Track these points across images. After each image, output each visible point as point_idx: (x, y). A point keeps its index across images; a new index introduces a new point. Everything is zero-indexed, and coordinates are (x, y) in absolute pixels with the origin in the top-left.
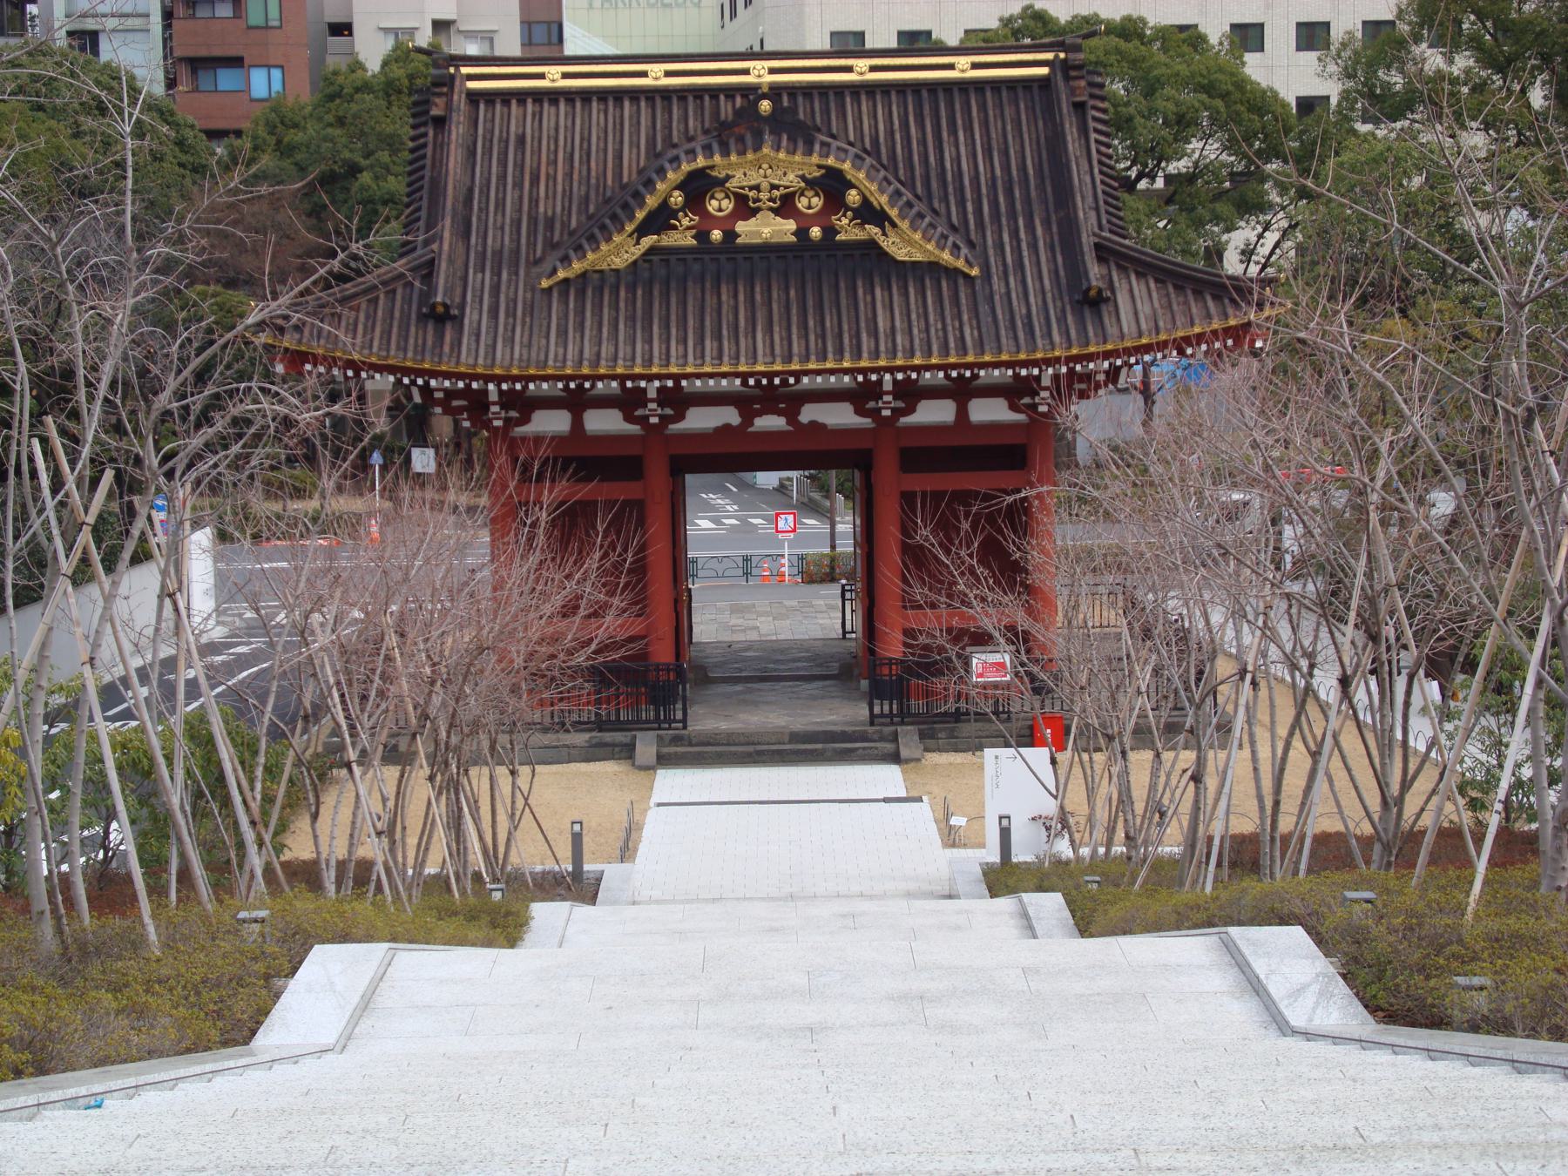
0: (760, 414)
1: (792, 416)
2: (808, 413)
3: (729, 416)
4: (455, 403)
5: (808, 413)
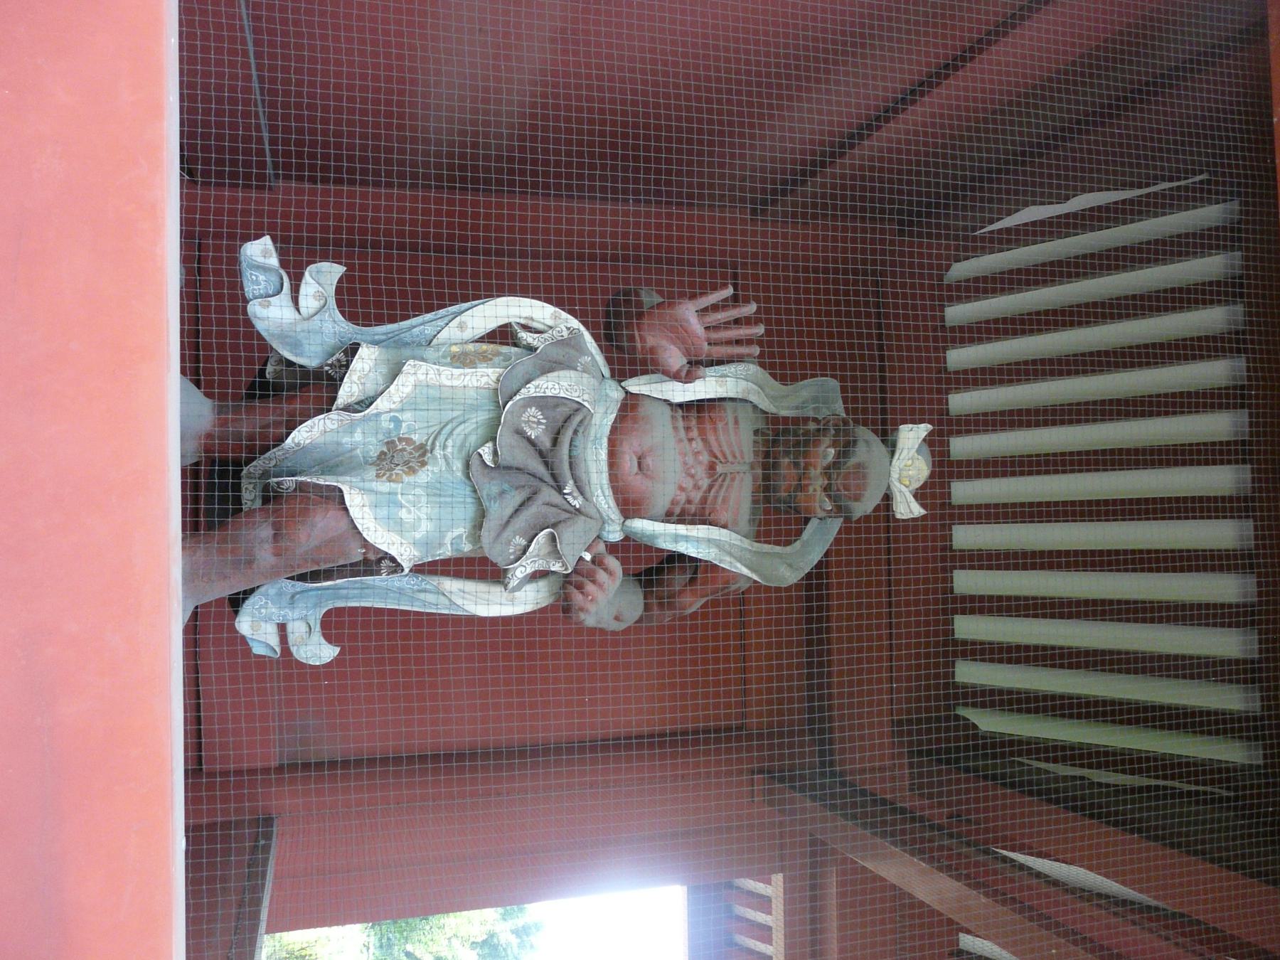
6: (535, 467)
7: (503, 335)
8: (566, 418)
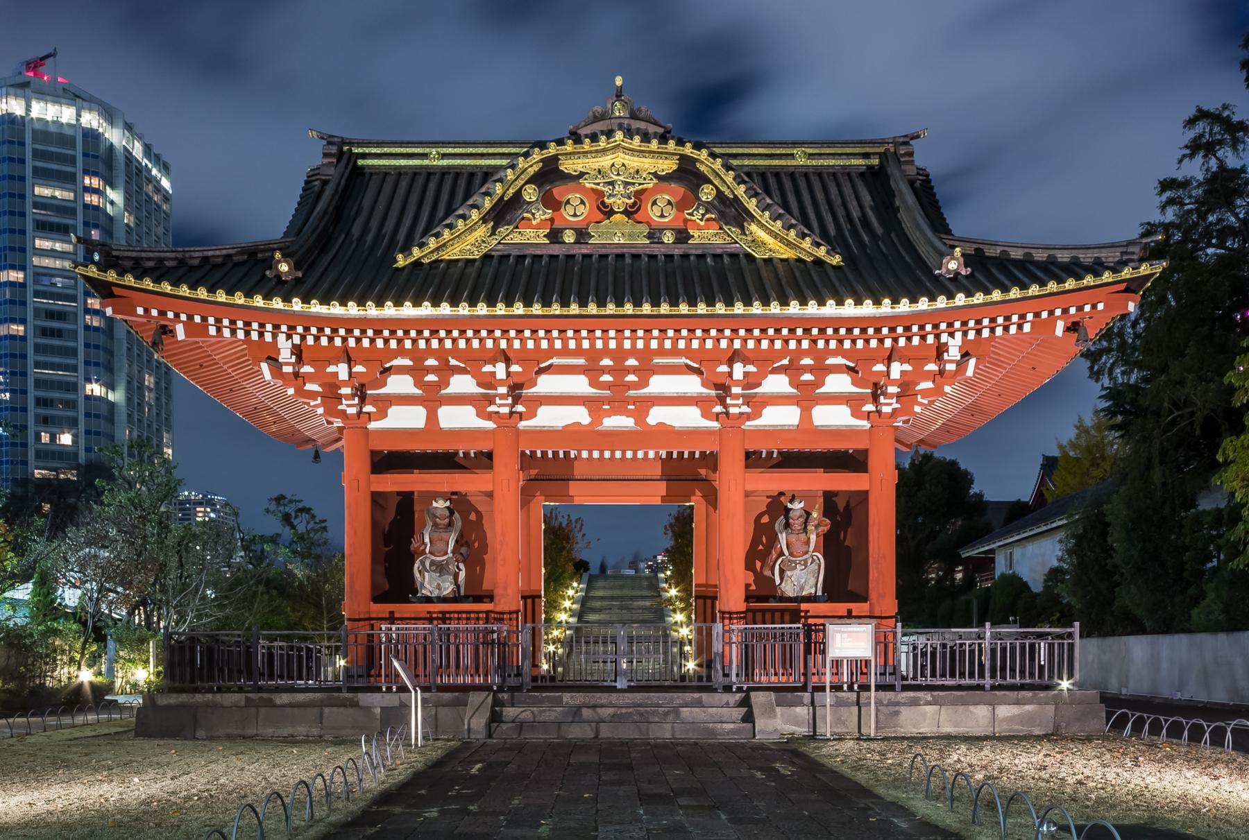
0: (609, 414)
1: (640, 415)
2: (657, 415)
3: (580, 415)
4: (310, 387)
5: (657, 415)
6: (440, 568)
7: (420, 572)
8: (433, 563)
